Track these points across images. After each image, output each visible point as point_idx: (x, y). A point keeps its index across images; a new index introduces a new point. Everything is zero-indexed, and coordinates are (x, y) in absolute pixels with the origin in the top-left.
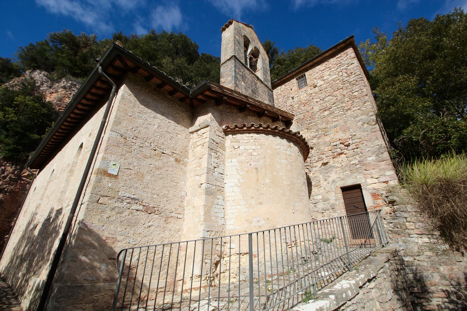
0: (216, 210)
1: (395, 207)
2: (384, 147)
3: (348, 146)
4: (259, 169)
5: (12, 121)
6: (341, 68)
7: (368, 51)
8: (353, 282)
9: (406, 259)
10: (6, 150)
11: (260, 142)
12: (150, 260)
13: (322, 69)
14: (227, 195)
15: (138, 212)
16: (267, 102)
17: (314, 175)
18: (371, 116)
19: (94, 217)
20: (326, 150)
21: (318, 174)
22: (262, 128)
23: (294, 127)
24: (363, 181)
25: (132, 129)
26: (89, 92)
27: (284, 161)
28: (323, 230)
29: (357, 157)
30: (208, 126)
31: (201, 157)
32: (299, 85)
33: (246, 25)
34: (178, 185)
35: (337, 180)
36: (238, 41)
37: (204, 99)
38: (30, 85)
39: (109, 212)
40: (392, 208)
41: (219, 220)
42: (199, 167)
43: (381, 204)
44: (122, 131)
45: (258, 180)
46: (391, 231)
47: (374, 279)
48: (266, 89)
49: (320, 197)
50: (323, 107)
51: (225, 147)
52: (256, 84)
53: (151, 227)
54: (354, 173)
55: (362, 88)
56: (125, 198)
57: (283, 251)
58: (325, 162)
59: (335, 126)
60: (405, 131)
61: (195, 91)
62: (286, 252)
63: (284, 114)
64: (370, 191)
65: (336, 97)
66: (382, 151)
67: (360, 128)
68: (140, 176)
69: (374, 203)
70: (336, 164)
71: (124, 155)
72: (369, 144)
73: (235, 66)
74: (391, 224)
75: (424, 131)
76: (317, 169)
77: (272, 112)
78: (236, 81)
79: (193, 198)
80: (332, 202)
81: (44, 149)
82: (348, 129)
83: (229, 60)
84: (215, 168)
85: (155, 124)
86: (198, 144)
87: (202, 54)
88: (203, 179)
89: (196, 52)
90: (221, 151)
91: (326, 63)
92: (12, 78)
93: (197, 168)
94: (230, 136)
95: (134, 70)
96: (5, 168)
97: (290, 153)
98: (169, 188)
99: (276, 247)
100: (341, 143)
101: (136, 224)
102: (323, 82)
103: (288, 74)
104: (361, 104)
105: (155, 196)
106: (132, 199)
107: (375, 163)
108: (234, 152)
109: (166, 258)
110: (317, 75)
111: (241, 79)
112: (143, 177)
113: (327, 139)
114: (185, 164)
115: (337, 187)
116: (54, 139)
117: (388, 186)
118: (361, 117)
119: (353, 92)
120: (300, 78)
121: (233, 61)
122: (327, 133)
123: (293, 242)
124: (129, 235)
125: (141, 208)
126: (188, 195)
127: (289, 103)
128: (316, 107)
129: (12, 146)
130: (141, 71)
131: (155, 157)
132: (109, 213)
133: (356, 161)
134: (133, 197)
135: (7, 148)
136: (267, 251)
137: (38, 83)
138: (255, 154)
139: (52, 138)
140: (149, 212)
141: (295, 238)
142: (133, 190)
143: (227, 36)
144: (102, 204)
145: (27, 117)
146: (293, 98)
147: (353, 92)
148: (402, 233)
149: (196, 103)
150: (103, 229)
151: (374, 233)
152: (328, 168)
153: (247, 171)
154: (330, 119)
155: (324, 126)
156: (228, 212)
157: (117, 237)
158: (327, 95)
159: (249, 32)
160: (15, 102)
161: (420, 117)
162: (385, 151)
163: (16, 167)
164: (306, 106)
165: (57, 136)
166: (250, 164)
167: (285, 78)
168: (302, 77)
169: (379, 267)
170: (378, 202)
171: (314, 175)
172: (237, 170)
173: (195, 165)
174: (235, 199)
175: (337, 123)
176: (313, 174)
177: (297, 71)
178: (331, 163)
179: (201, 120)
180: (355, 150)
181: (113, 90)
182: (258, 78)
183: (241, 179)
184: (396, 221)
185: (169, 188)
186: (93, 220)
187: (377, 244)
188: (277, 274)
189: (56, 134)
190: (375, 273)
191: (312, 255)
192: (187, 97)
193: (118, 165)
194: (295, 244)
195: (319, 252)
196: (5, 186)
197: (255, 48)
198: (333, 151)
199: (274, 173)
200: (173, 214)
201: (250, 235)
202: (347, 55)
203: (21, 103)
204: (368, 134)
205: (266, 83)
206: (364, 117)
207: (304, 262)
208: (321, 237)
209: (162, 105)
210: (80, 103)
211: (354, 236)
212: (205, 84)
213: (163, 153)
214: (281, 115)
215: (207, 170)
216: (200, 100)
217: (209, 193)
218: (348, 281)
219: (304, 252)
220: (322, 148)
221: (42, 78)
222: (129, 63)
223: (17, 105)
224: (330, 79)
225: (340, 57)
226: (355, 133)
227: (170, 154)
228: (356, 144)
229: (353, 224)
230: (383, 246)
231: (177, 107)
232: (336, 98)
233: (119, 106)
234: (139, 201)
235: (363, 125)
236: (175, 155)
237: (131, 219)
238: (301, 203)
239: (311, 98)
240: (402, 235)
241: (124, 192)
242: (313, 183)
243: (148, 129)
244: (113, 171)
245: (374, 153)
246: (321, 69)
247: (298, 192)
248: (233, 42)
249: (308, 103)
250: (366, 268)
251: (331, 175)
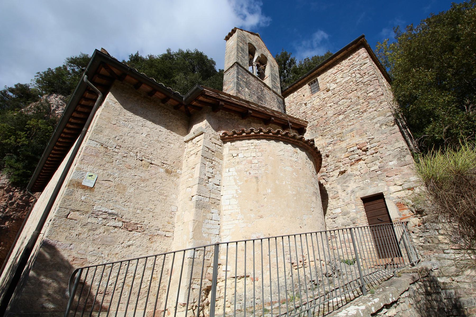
0: (208, 226)
1: (423, 217)
2: (406, 149)
3: (366, 150)
4: (260, 178)
5: (23, 145)
7: (386, 52)
8: (363, 307)
9: (441, 280)
10: (16, 175)
11: (261, 149)
12: (128, 285)
13: (334, 72)
14: (223, 209)
15: (116, 229)
18: (388, 116)
20: (342, 157)
21: (335, 185)
22: (263, 133)
23: (308, 134)
24: (386, 189)
25: (116, 137)
26: (79, 104)
27: (289, 169)
29: (377, 162)
30: (202, 134)
31: (194, 167)
34: (168, 198)
35: (356, 190)
36: (241, 48)
37: (199, 105)
40: (421, 219)
41: (212, 238)
42: (192, 177)
43: (408, 215)
44: (103, 140)
45: (258, 190)
46: (422, 246)
47: (395, 305)
48: (275, 96)
49: (339, 210)
50: (338, 111)
51: (223, 156)
52: (262, 91)
54: (375, 181)
56: (100, 213)
57: (287, 273)
58: (342, 170)
59: (351, 131)
63: (296, 121)
64: (394, 201)
65: (352, 102)
67: (378, 130)
69: (400, 214)
70: (354, 172)
71: (104, 166)
72: (389, 147)
73: (238, 73)
74: (421, 239)
75: (446, 128)
77: (281, 119)
78: (239, 88)
79: (183, 213)
80: (352, 216)
81: (42, 169)
82: (366, 132)
83: (231, 67)
84: (209, 178)
86: (192, 153)
88: (194, 191)
91: (338, 65)
92: (29, 104)
93: (189, 179)
94: (229, 143)
95: (121, 78)
96: (13, 194)
97: (296, 160)
98: (156, 202)
100: (358, 149)
102: (336, 85)
106: (110, 214)
107: (397, 168)
110: (330, 78)
111: (244, 86)
112: (124, 190)
113: (344, 145)
114: (177, 176)
115: (357, 198)
118: (378, 119)
119: (368, 92)
120: (312, 84)
121: (235, 67)
122: (343, 139)
123: (301, 262)
124: (103, 255)
125: (120, 224)
127: (302, 110)
128: (330, 112)
129: (21, 171)
130: (128, 78)
131: (141, 168)
132: (79, 229)
133: (376, 167)
134: (110, 211)
135: (17, 173)
137: (53, 107)
138: (256, 161)
139: (49, 156)
140: (130, 229)
141: (303, 257)
142: (112, 204)
144: (71, 219)
146: (306, 104)
147: (368, 92)
148: (435, 248)
149: (192, 110)
150: (70, 248)
151: (401, 250)
152: (346, 177)
153: (246, 181)
154: (345, 123)
155: (339, 131)
156: (223, 228)
157: (88, 257)
158: (341, 98)
160: (27, 126)
161: (441, 112)
162: (408, 154)
163: (24, 192)
165: (54, 154)
167: (297, 85)
168: (315, 82)
169: (401, 290)
170: (404, 213)
172: (235, 180)
173: (187, 176)
174: (232, 213)
175: (352, 127)
176: (330, 184)
177: (309, 76)
178: (349, 172)
179: (196, 127)
180: (374, 155)
181: (99, 99)
182: (265, 85)
183: (239, 190)
185: (156, 202)
186: (59, 237)
188: (279, 301)
189: (53, 151)
190: (395, 297)
191: (325, 277)
192: (181, 104)
193: (95, 177)
196: (11, 213)
198: (350, 157)
200: (159, 232)
201: (217, 245)
202: (359, 56)
203: (33, 126)
204: (387, 137)
205: (274, 90)
206: (381, 118)
207: (314, 286)
211: (381, 254)
212: (197, 88)
213: (151, 164)
214: (290, 122)
215: (199, 180)
216: (194, 107)
217: (200, 206)
218: (357, 307)
219: (313, 274)
220: (338, 155)
221: (58, 102)
222: (115, 71)
223: (29, 129)
224: (343, 81)
225: (352, 58)
226: (372, 137)
227: (160, 164)
228: (374, 148)
229: (378, 240)
230: (413, 265)
231: (171, 115)
232: (350, 101)
233: (101, 114)
234: (118, 216)
236: (165, 165)
237: (107, 237)
238: (311, 216)
239: (324, 102)
240: (435, 250)
241: (99, 206)
242: (330, 195)
245: (395, 157)
246: (333, 72)
247: (306, 203)
249: (322, 108)
250: (384, 291)
251: (350, 185)
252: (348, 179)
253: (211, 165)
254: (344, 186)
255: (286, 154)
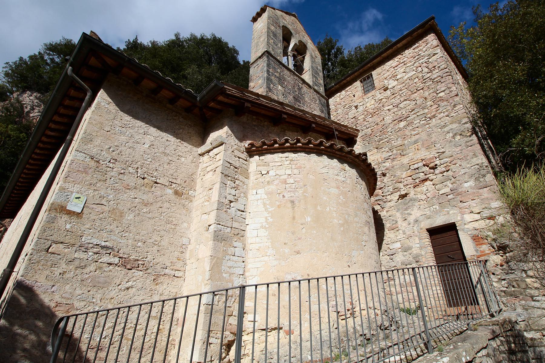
0: (230, 264)
1: (507, 255)
2: (487, 166)
3: (434, 168)
4: (296, 202)
6: (420, 62)
9: (528, 335)
13: (394, 65)
14: (249, 242)
15: (111, 267)
16: (317, 112)
17: (389, 214)
19: (39, 272)
20: (404, 176)
22: (300, 144)
23: (359, 147)
24: (459, 218)
25: (110, 148)
27: (334, 191)
28: (405, 294)
30: (222, 144)
31: (211, 187)
32: (364, 89)
33: (286, 13)
34: (178, 228)
35: (421, 218)
36: (273, 33)
38: (16, 111)
39: (64, 266)
40: (504, 257)
41: (234, 279)
42: (208, 201)
43: (487, 252)
45: (294, 218)
46: (504, 292)
48: (316, 96)
49: (398, 245)
51: (248, 174)
52: (300, 89)
53: (130, 289)
54: (445, 207)
55: (449, 86)
56: (91, 245)
57: (331, 324)
58: (403, 193)
59: (416, 142)
60: (514, 141)
61: (204, 96)
62: (336, 326)
63: (343, 129)
66: (483, 172)
68: (117, 215)
69: (477, 251)
72: (464, 164)
73: (268, 65)
74: (503, 282)
75: (539, 139)
76: (392, 204)
78: (269, 85)
79: (197, 247)
80: (415, 252)
82: (434, 143)
83: (260, 57)
84: (231, 202)
85: (145, 141)
86: (209, 169)
87: (244, 61)
88: (212, 218)
89: (235, 59)
90: (241, 178)
91: (399, 56)
93: (206, 204)
94: (256, 157)
97: (343, 179)
98: (162, 233)
99: (320, 318)
100: (424, 165)
101: (106, 284)
102: (396, 83)
103: (349, 76)
104: (449, 108)
105: (139, 243)
106: (103, 247)
107: (475, 191)
108: (261, 179)
109: (150, 338)
110: (388, 73)
111: (277, 82)
112: (121, 216)
113: (405, 160)
114: (190, 199)
115: (421, 229)
116: (25, 174)
117: (495, 223)
118: (451, 127)
119: (438, 92)
120: (365, 80)
121: (265, 58)
122: (405, 153)
123: (348, 310)
124: (94, 300)
125: (116, 260)
126: (191, 242)
128: (388, 117)
130: (125, 70)
131: (143, 188)
132: (63, 266)
133: (447, 190)
134: (103, 244)
136: (306, 325)
137: (26, 108)
138: (292, 181)
140: (128, 267)
141: (352, 304)
142: (105, 235)
143: (259, 27)
144: (53, 253)
145: (8, 152)
146: (356, 107)
147: (438, 92)
148: (521, 294)
150: (52, 290)
151: (478, 296)
152: (407, 201)
153: (279, 206)
154: (407, 133)
155: (399, 142)
156: (249, 266)
157: (75, 303)
158: (402, 99)
159: (289, 21)
162: (488, 172)
164: (375, 117)
165: (29, 169)
166: (284, 196)
167: (345, 81)
168: (368, 78)
169: (477, 347)
170: (482, 249)
171: (389, 214)
172: (265, 205)
173: (203, 200)
176: (387, 212)
179: (214, 136)
180: (445, 174)
182: (304, 82)
183: (269, 218)
184: (512, 276)
185: (162, 233)
186: (37, 277)
187: (485, 312)
189: (27, 166)
190: (469, 355)
191: (379, 330)
194: (351, 314)
195: (394, 327)
197: (300, 42)
199: (319, 208)
200: (167, 271)
202: (427, 44)
204: (461, 150)
205: (316, 88)
206: (454, 126)
208: (402, 306)
209: (158, 117)
210: (51, 121)
213: (156, 183)
214: (337, 130)
215: (218, 204)
216: (212, 109)
217: (218, 237)
220: (398, 173)
221: (33, 102)
222: (109, 61)
224: (406, 78)
226: (443, 150)
227: (167, 184)
228: (445, 165)
229: (449, 283)
231: (181, 120)
234: (114, 251)
235: (453, 137)
236: (174, 185)
239: (381, 105)
240: (521, 297)
241: (89, 238)
242: (387, 225)
243: (134, 149)
244: (75, 206)
245: (471, 176)
246: (393, 65)
247: (356, 235)
248: (266, 34)
249: (377, 113)
251: (412, 212)
252: (410, 204)
253: (234, 185)
254: (405, 214)
255: (331, 171)
